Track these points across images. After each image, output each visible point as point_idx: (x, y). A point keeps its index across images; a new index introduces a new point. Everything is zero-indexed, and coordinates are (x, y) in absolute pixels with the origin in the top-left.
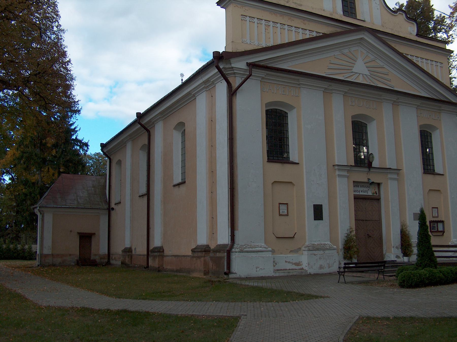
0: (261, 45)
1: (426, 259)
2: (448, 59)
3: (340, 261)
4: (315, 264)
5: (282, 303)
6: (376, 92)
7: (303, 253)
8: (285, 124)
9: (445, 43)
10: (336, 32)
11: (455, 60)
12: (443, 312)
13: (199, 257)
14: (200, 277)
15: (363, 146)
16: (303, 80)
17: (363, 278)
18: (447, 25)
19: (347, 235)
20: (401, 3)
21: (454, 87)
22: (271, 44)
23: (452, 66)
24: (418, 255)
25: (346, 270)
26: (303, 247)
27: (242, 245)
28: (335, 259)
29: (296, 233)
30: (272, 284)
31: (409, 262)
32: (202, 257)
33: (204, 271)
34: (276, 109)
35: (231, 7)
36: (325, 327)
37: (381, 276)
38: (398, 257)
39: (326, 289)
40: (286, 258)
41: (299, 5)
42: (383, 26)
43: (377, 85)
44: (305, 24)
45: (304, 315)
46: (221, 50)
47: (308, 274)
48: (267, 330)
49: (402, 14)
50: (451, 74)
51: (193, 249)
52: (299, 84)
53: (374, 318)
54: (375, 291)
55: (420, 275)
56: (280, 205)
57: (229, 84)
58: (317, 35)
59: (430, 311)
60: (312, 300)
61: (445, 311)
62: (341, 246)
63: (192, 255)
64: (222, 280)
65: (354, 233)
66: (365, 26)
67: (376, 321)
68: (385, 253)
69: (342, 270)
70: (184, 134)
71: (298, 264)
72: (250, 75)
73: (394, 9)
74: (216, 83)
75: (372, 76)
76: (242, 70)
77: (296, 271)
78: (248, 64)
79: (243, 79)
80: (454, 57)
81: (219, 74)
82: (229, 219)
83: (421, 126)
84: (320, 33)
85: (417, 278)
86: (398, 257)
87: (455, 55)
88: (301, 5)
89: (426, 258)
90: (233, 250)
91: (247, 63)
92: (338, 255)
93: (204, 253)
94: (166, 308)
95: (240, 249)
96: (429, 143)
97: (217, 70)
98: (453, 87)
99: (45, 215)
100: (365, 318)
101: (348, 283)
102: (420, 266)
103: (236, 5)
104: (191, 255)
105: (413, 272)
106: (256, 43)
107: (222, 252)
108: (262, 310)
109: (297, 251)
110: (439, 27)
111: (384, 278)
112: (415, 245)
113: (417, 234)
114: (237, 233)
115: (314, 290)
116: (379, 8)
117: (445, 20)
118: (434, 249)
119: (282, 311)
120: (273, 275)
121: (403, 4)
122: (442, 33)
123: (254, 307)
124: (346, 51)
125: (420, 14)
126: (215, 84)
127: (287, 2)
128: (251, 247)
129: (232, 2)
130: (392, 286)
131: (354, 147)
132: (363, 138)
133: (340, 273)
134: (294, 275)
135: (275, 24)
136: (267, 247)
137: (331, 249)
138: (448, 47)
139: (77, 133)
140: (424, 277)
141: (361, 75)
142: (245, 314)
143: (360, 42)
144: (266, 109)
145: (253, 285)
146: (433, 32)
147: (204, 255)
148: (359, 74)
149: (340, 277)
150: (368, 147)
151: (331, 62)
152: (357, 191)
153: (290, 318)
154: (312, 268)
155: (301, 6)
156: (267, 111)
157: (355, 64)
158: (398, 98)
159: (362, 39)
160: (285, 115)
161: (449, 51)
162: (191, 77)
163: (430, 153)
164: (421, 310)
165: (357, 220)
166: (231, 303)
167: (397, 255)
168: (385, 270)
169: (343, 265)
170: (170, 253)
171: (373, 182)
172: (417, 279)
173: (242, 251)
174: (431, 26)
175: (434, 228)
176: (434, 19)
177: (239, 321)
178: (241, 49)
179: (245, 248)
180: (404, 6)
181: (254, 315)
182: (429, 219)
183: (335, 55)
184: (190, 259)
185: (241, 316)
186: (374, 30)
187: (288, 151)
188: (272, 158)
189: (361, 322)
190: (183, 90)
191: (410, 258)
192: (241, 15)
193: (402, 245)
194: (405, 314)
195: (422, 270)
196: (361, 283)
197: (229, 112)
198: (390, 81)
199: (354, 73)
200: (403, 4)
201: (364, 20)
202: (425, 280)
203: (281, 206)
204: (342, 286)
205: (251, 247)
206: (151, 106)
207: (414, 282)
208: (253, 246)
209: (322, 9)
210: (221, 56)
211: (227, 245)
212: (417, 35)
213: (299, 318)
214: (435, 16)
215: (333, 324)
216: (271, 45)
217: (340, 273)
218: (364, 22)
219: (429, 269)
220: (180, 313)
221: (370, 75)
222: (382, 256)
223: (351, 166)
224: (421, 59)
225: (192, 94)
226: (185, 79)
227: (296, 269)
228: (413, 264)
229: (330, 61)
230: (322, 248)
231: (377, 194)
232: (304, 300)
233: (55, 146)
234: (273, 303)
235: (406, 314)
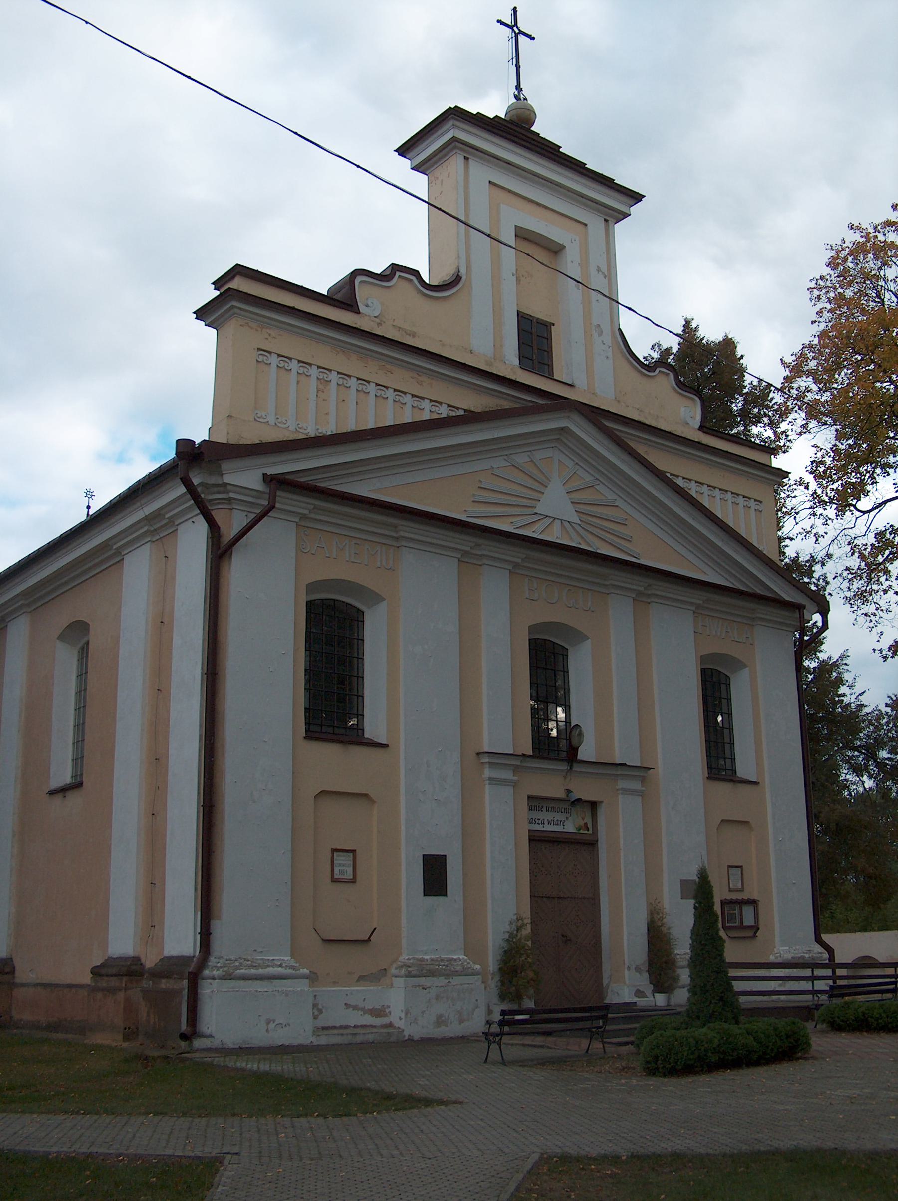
0: (305, 430)
1: (713, 1001)
2: (776, 491)
3: (489, 1007)
4: (423, 1012)
5: (335, 1119)
7: (392, 985)
8: (356, 641)
9: (769, 453)
10: (500, 409)
11: (793, 495)
12: (756, 1139)
13: (113, 991)
14: (114, 1044)
15: (555, 705)
16: (408, 529)
17: (551, 1050)
18: (776, 407)
19: (509, 937)
20: (664, 346)
21: (787, 560)
22: (330, 429)
23: (784, 510)
24: (693, 991)
25: (506, 1029)
26: (394, 966)
27: (230, 960)
28: (477, 1000)
29: (375, 929)
30: (309, 1066)
31: (668, 1006)
32: (120, 990)
33: (125, 1029)
34: (334, 600)
35: (232, 326)
36: (450, 1184)
37: (597, 1045)
38: (639, 993)
39: (452, 1081)
40: (347, 995)
41: (410, 335)
42: (619, 402)
43: (597, 549)
44: (420, 383)
45: (395, 1152)
46: (199, 435)
47: (406, 1038)
48: (295, 1196)
49: (667, 374)
50: (781, 530)
51: (98, 966)
52: (397, 539)
53: (578, 1159)
54: (581, 1086)
55: (697, 1042)
56: (730, 869)
57: (213, 526)
58: (451, 415)
59: (723, 1135)
60: (415, 1111)
61: (760, 1135)
62: (492, 963)
63: (93, 984)
64: (173, 1054)
65: (527, 931)
66: (573, 398)
67: (585, 1167)
68: (608, 985)
69: (495, 1028)
70: (84, 652)
71: (378, 1012)
72: (271, 508)
73: (646, 360)
74: (180, 524)
77: (374, 1030)
78: (268, 479)
79: (252, 516)
80: (790, 486)
81: (190, 500)
82: (196, 889)
83: (703, 659)
84: (458, 409)
85: (690, 1049)
86: (639, 993)
87: (792, 482)
88: (413, 334)
89: (714, 998)
90: (206, 972)
91: (263, 474)
92: (485, 988)
93: (125, 979)
94: (15, 1133)
95: (226, 969)
96: (724, 702)
97: (183, 490)
98: (785, 561)
100: (555, 1159)
101: (513, 1063)
102: (698, 1017)
103: (247, 321)
104: (89, 983)
105: (679, 1034)
106: (292, 425)
107: (175, 976)
108: (281, 1139)
109: (378, 976)
110: (756, 410)
111: (604, 1050)
112: (685, 963)
113: (690, 936)
114: (218, 929)
115: (420, 1082)
116: (610, 355)
117: (771, 395)
118: (733, 973)
119: (335, 1141)
120: (311, 1042)
121: (671, 347)
122: (763, 425)
123: (259, 1131)
124: (521, 459)
125: (711, 375)
126: (177, 525)
127: (379, 324)
128: (256, 966)
129: (235, 313)
130: (626, 1070)
131: (532, 708)
132: (557, 684)
133: (491, 1038)
134: (368, 1043)
135: (343, 378)
136: (298, 965)
137: (466, 972)
138: (777, 462)
140: (706, 1045)
142: (236, 1149)
143: (558, 439)
144: (309, 599)
145: (259, 1068)
146: (740, 421)
147: (126, 985)
148: (552, 520)
149: (489, 1047)
150: (567, 707)
151: (482, 486)
152: (537, 822)
153: (358, 1161)
154: (417, 1023)
156: (310, 605)
157: (543, 493)
158: (649, 585)
159: (563, 430)
160: (358, 618)
161: (778, 471)
162: (113, 503)
163: (724, 726)
164: (701, 1135)
165: (535, 897)
166: (197, 1120)
167: (638, 989)
168: (607, 1028)
169: (497, 1017)
170: (32, 977)
171: (579, 800)
172: (690, 1051)
173: (231, 975)
174: (737, 406)
175: (732, 918)
176: (745, 391)
177: (217, 1171)
178: (251, 436)
179: (237, 968)
180: (672, 353)
181: (260, 1152)
182: (719, 894)
183: (492, 468)
184: (86, 994)
185: (225, 1155)
186: (594, 410)
187: (360, 712)
188: (318, 729)
189: (545, 1170)
190: (113, 523)
191: (672, 996)
192: (258, 348)
193: (651, 962)
194: (659, 1146)
195: (703, 1028)
196: (543, 1064)
197: (210, 602)
198: (631, 541)
199: (536, 518)
200: (671, 347)
201: (570, 383)
202: (710, 1054)
203: (338, 856)
204: (495, 1073)
205: (254, 964)
206: (128, 487)
207: (682, 1058)
208: (260, 962)
209: (466, 349)
210: (196, 451)
211: (190, 959)
212: (701, 428)
213: (382, 1161)
214: (746, 383)
215: (472, 1178)
216: (329, 433)
217: (491, 1038)
218: (569, 388)
219: (720, 1027)
220: (55, 1149)
221: (579, 522)
222: (600, 990)
223: (524, 755)
224: (709, 488)
225: (112, 547)
226: (99, 503)
227: (375, 1027)
228: (679, 1013)
229: (481, 482)
230: (444, 970)
232: (393, 1110)
234: (312, 1120)
235: (663, 1145)
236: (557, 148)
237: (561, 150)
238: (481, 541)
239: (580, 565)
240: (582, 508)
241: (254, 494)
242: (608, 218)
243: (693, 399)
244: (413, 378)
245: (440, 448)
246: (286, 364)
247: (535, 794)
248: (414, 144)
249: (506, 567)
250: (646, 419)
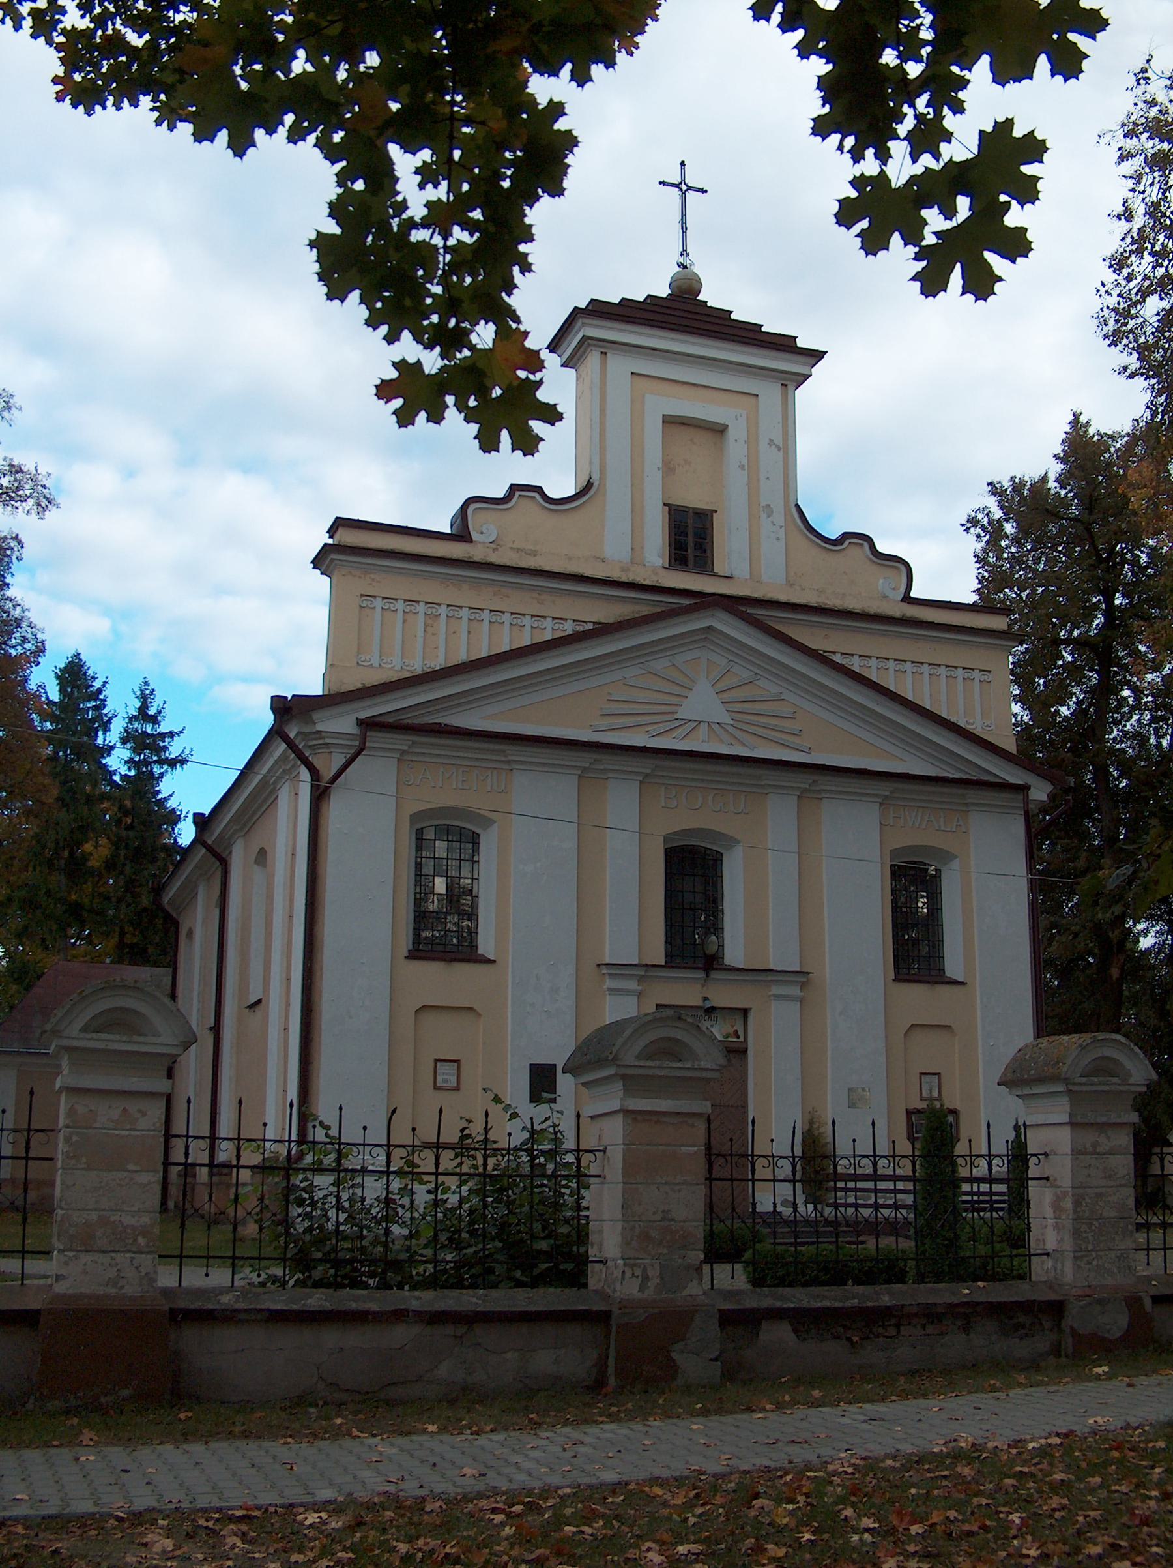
6: (734, 770)
16: (515, 752)
41: (530, 554)
49: (862, 545)
56: (923, 1077)
57: (314, 772)
78: (361, 723)
88: (534, 554)
127: (494, 550)
139: (179, 826)
141: (704, 726)
155: (535, 556)
159: (710, 629)
199: (677, 723)
221: (732, 722)
229: (610, 694)
231: (738, 1037)
233: (111, 865)
236: (757, 328)
237: (763, 329)
239: (718, 768)
241: (351, 737)
243: (896, 568)
244: (533, 598)
247: (663, 1002)
249: (635, 778)
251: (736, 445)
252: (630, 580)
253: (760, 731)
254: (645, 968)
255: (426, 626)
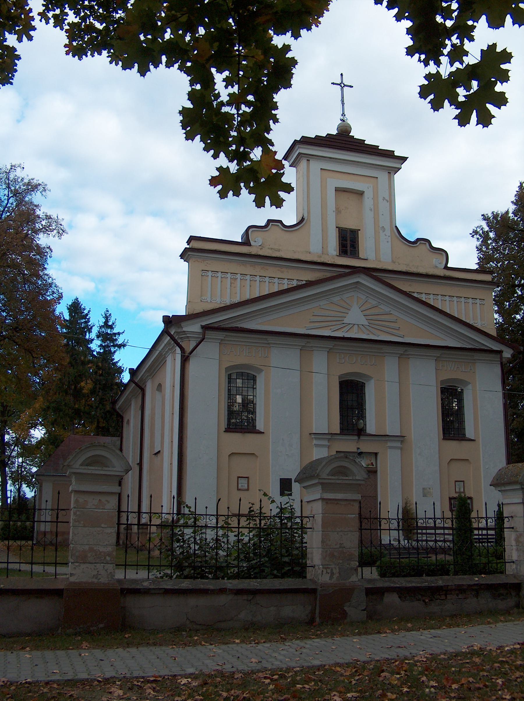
16: (271, 339)
42: (394, 262)
44: (282, 272)
52: (269, 344)
56: (239, 479)
72: (204, 339)
75: (370, 325)
76: (196, 333)
78: (203, 327)
99: (44, 485)
106: (218, 300)
127: (261, 249)
141: (356, 326)
155: (279, 251)
159: (358, 282)
221: (368, 324)
231: (373, 465)
237: (379, 148)
238: (308, 340)
240: (368, 317)
241: (198, 333)
242: (390, 172)
243: (441, 254)
244: (278, 270)
245: (329, 290)
246: (216, 275)
248: (288, 156)
250: (410, 268)
251: (368, 200)
252: (322, 261)
253: (382, 328)
254: (331, 435)
255: (231, 283)
